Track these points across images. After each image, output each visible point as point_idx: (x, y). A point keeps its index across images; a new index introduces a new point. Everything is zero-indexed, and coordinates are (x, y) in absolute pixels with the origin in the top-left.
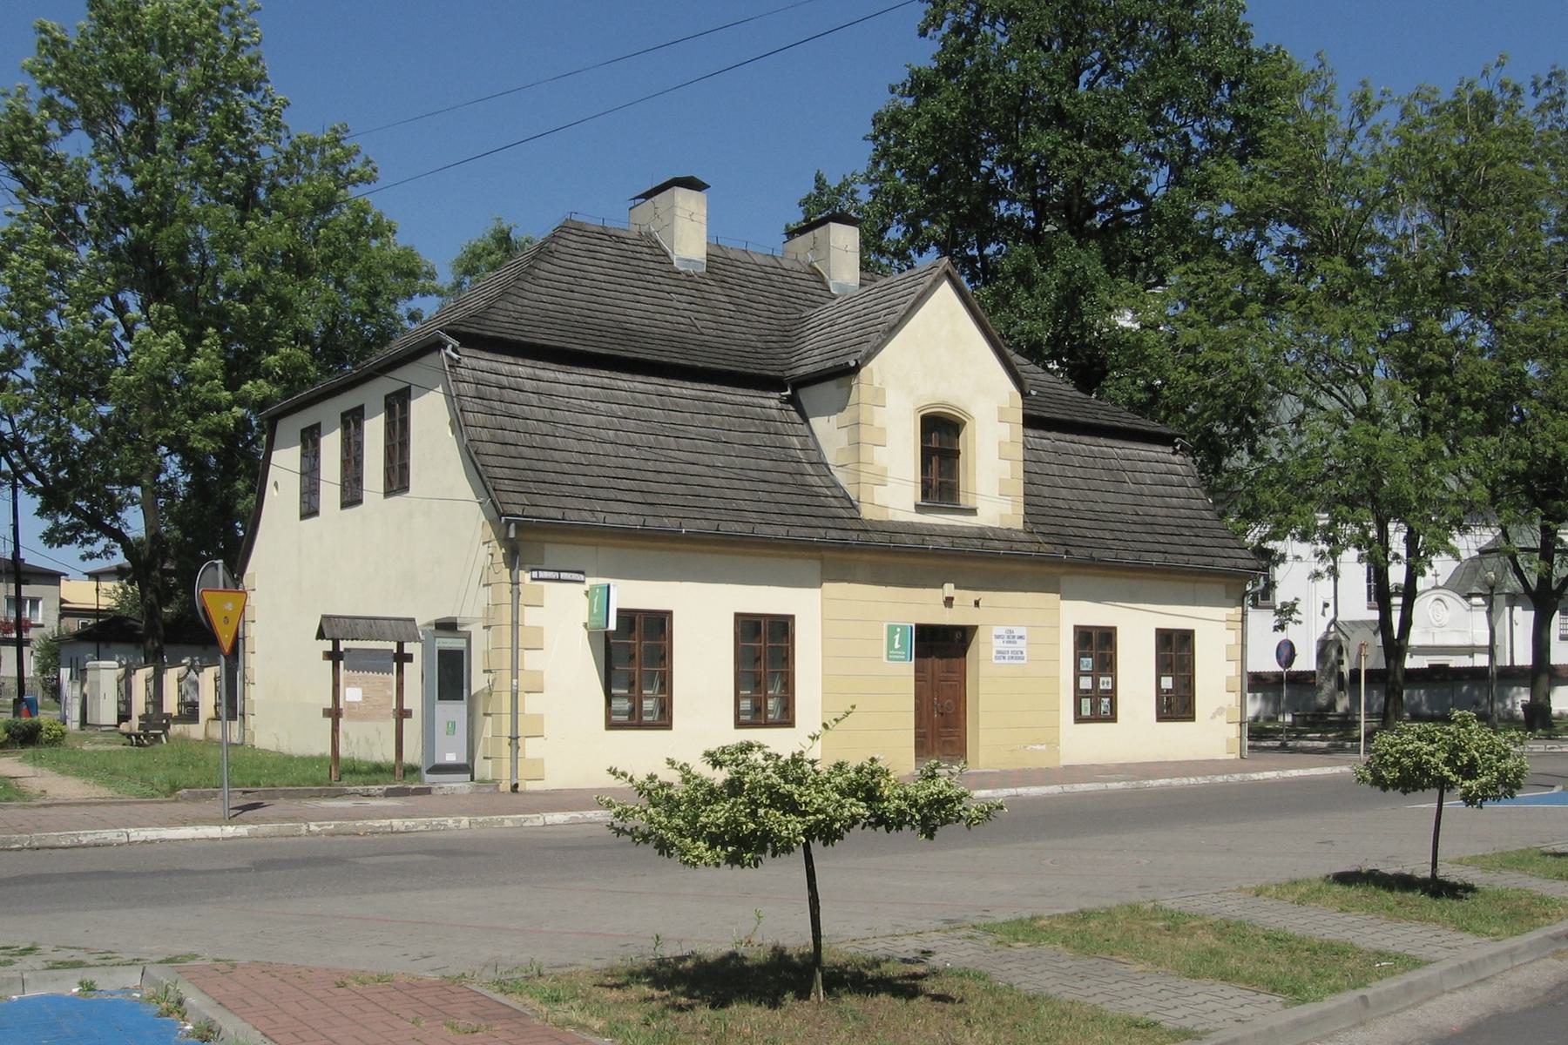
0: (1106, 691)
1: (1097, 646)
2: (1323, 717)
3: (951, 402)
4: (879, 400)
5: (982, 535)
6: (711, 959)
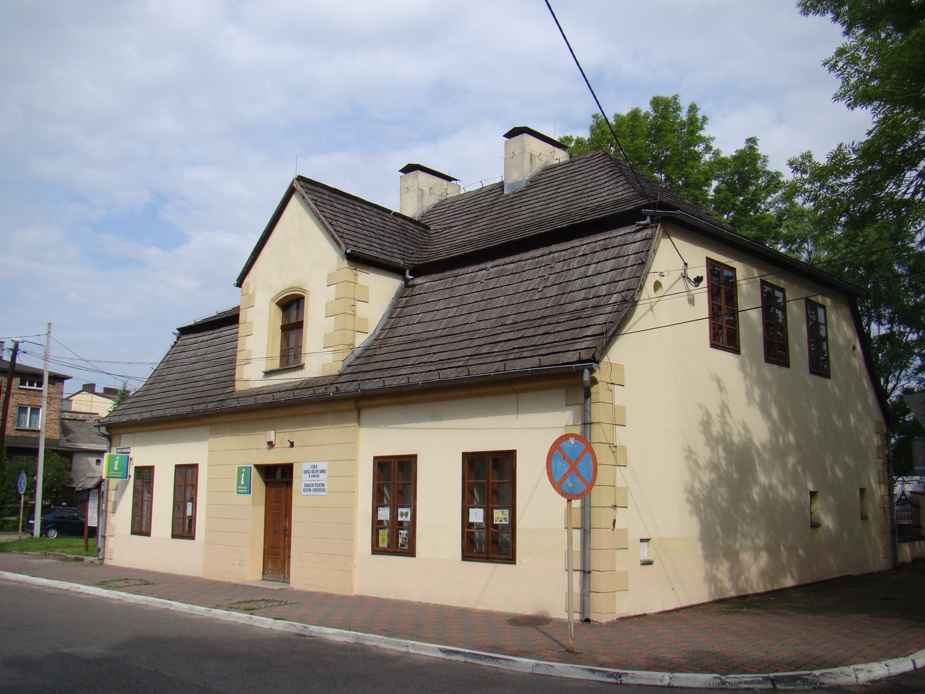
1: (396, 478)
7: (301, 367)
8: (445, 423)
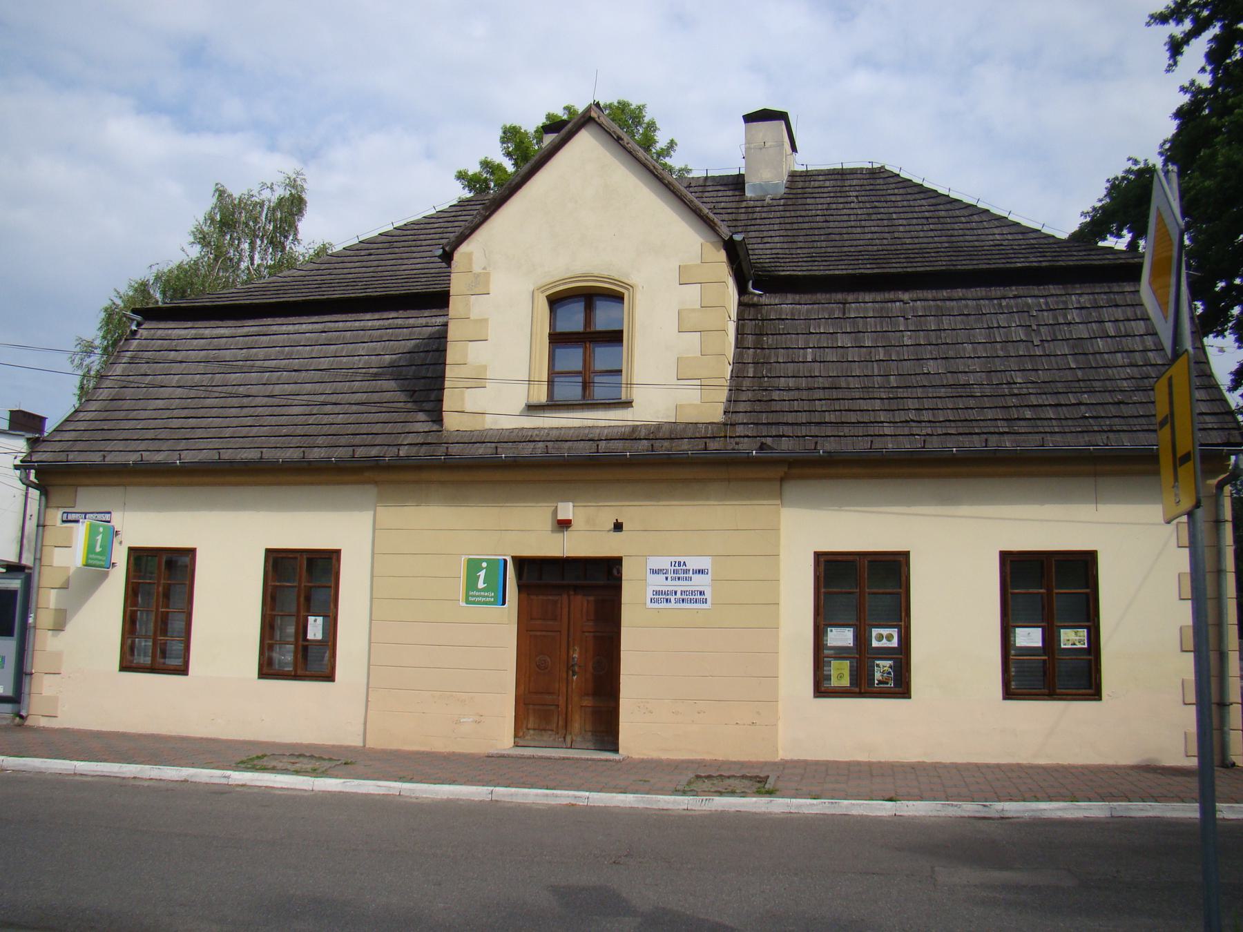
4: (481, 287)
5: (655, 433)
6: (636, 756)
7: (628, 404)
8: (965, 510)
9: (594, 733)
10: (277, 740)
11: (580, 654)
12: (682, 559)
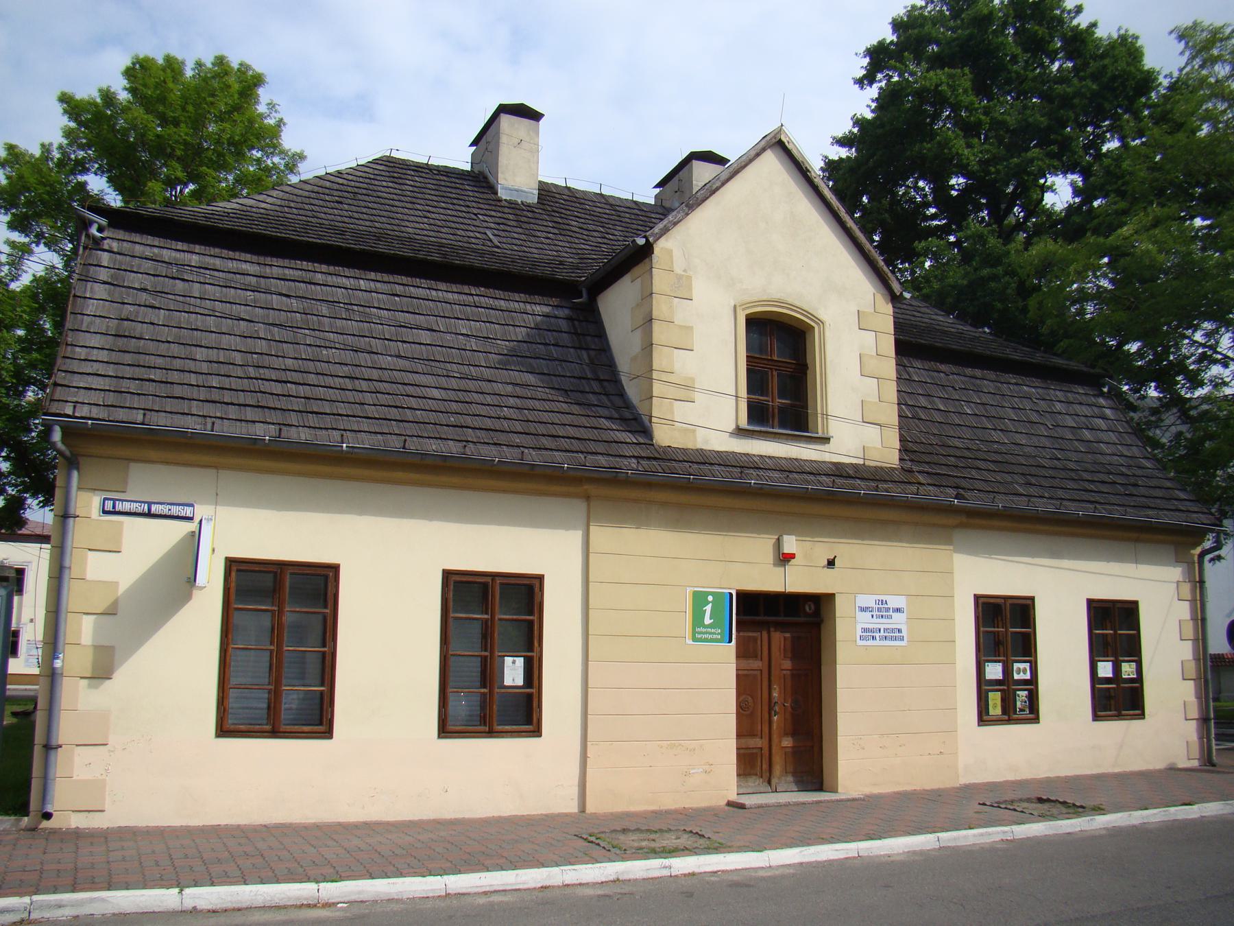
0: (1025, 682)
1: (1006, 627)
2: (98, 244)
3: (790, 301)
5: (839, 471)
7: (826, 440)
8: (1066, 563)
9: (794, 774)
10: (467, 815)
11: (780, 693)
12: (884, 598)
